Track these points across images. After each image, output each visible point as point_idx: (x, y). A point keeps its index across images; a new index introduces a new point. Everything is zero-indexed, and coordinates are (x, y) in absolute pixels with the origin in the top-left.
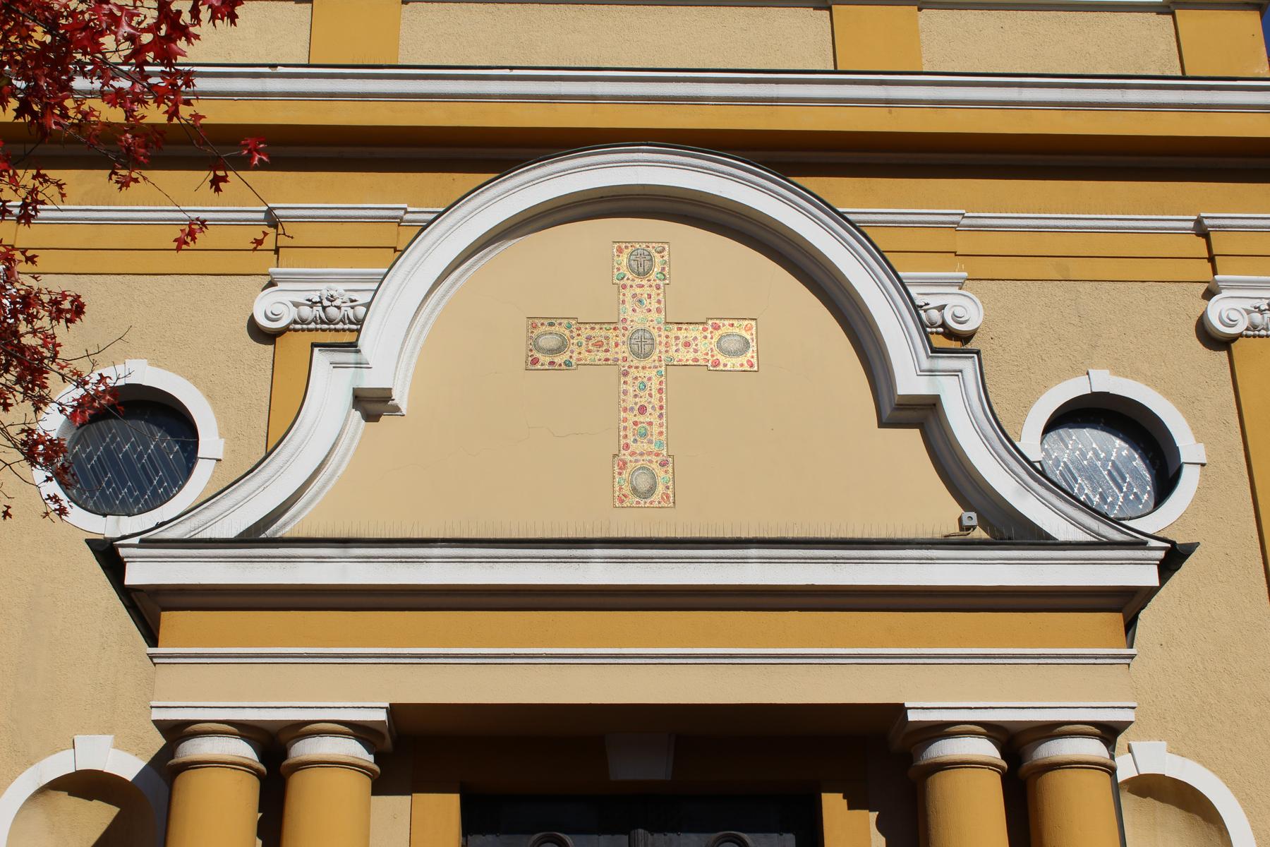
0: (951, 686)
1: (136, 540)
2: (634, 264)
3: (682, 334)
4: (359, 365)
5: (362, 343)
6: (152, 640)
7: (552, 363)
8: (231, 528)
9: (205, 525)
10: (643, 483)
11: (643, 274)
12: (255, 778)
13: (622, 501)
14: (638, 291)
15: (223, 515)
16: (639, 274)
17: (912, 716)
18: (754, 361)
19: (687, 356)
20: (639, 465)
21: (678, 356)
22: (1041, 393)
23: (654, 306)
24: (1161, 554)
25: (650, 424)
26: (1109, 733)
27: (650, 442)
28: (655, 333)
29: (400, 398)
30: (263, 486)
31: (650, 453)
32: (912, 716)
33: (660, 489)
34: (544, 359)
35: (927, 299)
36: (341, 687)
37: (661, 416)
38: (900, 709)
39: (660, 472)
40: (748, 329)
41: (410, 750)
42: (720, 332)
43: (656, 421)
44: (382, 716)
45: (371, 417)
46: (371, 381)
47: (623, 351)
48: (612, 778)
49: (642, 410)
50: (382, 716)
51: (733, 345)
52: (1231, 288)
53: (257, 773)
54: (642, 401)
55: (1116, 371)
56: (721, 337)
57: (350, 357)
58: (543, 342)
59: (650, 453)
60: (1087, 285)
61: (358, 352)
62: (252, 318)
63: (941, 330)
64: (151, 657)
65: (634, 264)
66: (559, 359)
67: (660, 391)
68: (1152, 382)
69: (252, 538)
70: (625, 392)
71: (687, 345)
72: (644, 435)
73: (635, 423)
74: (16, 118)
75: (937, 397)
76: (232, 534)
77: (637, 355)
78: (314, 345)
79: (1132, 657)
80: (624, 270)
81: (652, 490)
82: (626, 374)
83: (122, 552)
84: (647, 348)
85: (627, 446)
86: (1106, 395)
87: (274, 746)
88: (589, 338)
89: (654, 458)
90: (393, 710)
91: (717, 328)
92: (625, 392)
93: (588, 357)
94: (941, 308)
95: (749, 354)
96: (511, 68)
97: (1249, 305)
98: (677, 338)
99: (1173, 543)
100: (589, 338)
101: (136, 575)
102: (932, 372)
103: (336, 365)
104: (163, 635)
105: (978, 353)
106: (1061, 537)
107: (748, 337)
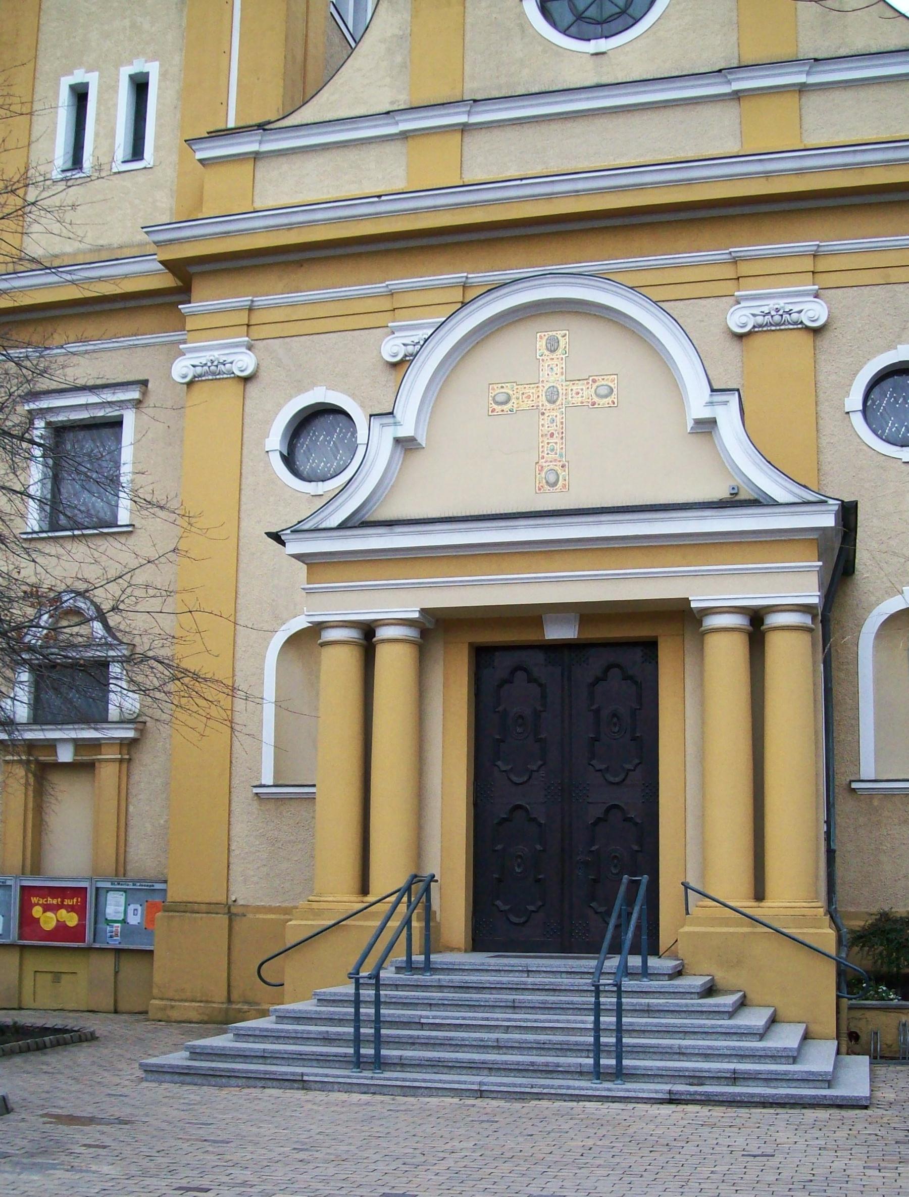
1: (288, 531)
2: (549, 345)
3: (574, 388)
4: (395, 424)
8: (335, 521)
9: (322, 520)
10: (552, 479)
11: (553, 351)
12: (356, 648)
13: (540, 489)
14: (550, 362)
15: (331, 514)
16: (551, 351)
17: (693, 605)
18: (616, 401)
19: (577, 400)
21: (574, 401)
22: (865, 363)
23: (559, 371)
24: (836, 508)
31: (555, 460)
34: (498, 408)
35: (790, 307)
36: (396, 603)
37: (562, 438)
39: (562, 474)
42: (597, 384)
43: (559, 441)
44: (416, 615)
46: (406, 431)
48: (547, 638)
49: (552, 435)
54: (551, 430)
56: (598, 387)
57: (388, 420)
58: (498, 399)
59: (555, 460)
60: (901, 286)
61: (394, 417)
62: (387, 362)
63: (800, 326)
66: (506, 407)
67: (562, 423)
69: (342, 526)
70: (543, 425)
71: (578, 393)
72: (552, 450)
73: (548, 443)
81: (555, 483)
82: (543, 414)
84: (555, 397)
85: (543, 457)
87: (368, 632)
89: (558, 463)
90: (423, 611)
91: (594, 381)
92: (543, 425)
93: (524, 406)
94: (800, 312)
95: (613, 396)
99: (843, 501)
102: (711, 403)
103: (383, 425)
105: (738, 390)
106: (780, 500)
107: (612, 386)
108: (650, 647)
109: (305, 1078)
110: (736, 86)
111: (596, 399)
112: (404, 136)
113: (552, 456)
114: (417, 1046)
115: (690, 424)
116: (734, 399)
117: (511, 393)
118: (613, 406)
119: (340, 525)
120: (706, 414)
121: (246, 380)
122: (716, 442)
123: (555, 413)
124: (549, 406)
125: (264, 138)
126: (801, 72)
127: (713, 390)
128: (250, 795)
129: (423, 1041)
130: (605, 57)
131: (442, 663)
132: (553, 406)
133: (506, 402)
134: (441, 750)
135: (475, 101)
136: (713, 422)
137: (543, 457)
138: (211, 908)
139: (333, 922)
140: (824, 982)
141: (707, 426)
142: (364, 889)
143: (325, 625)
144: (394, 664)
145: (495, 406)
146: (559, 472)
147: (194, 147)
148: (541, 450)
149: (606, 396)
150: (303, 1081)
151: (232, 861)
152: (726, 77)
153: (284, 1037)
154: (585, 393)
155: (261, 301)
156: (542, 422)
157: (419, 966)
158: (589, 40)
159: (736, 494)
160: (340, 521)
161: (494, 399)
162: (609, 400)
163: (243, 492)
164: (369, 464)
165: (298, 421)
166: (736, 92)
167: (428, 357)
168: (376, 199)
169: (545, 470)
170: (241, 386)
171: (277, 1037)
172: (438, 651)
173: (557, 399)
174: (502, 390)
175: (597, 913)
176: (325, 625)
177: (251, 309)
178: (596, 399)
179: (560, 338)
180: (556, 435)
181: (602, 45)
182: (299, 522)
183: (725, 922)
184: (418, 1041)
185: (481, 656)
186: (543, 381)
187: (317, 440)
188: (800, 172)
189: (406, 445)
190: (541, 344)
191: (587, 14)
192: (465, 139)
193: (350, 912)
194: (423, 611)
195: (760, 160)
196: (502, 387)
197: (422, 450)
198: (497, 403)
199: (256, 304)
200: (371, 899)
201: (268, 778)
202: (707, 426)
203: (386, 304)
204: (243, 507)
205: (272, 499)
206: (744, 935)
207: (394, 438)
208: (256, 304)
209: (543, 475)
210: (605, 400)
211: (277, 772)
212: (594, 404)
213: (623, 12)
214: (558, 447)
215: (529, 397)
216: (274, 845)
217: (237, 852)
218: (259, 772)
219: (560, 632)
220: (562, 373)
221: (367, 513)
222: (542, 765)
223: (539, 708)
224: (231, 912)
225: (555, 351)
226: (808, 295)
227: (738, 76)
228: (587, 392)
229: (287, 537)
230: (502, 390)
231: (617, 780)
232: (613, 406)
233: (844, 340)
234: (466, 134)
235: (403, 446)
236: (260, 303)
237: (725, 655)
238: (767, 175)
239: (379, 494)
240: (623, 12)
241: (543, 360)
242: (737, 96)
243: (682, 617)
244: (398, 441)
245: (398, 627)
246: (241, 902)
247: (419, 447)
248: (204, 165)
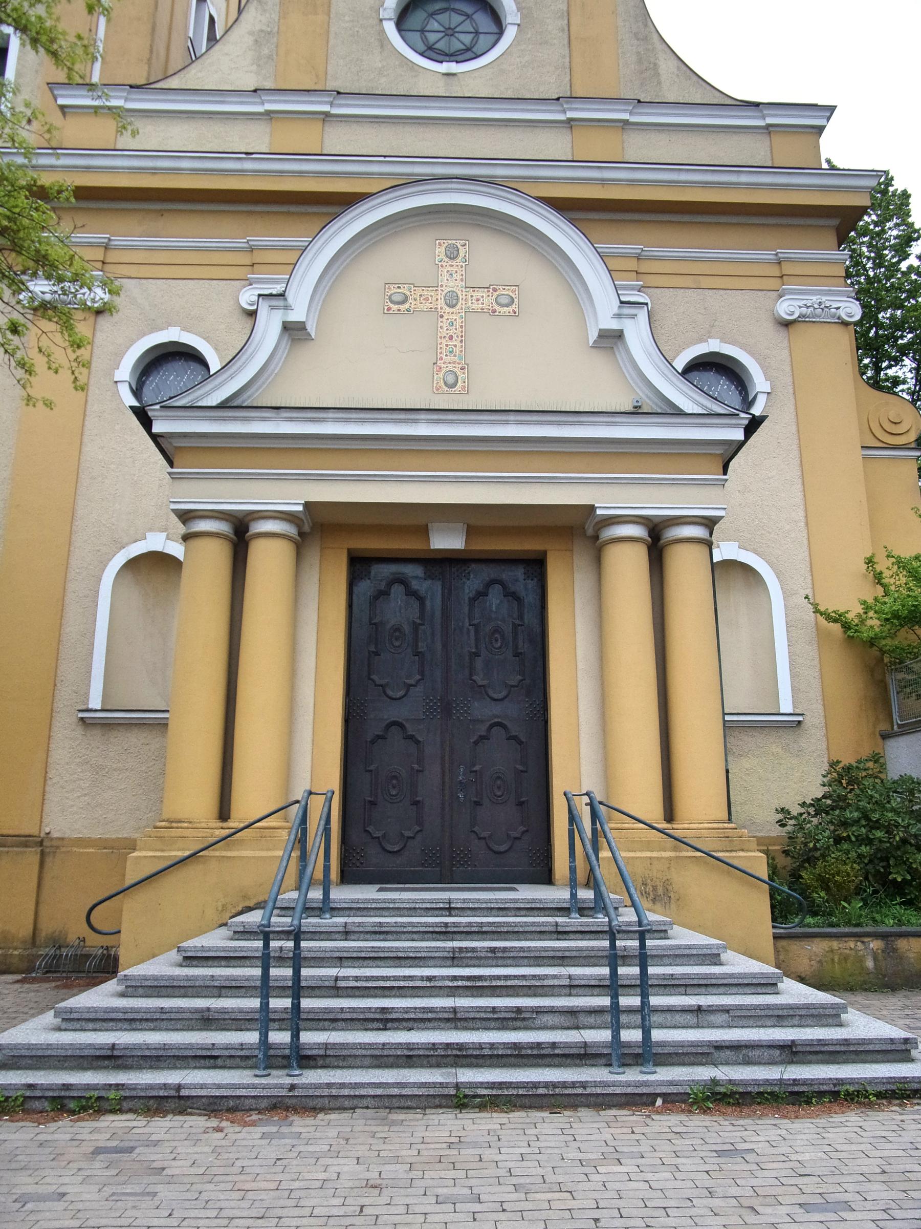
0: (622, 498)
1: (157, 407)
2: (448, 253)
5: (290, 295)
6: (171, 464)
7: (399, 310)
8: (215, 399)
9: (202, 397)
13: (438, 390)
15: (208, 394)
18: (517, 310)
19: (477, 306)
20: (448, 369)
23: (459, 277)
24: (746, 422)
25: (455, 346)
26: (710, 523)
27: (455, 356)
28: (459, 293)
29: (311, 328)
30: (231, 377)
31: (454, 363)
32: (599, 512)
33: (460, 384)
34: (395, 307)
37: (461, 341)
38: (592, 508)
39: (461, 376)
40: (513, 291)
41: (316, 527)
43: (459, 344)
44: (300, 508)
45: (294, 341)
47: (441, 303)
49: (451, 338)
50: (300, 508)
51: (504, 300)
52: (791, 293)
53: (231, 541)
55: (723, 340)
57: (280, 303)
58: (394, 298)
60: (710, 291)
61: (286, 299)
64: (169, 474)
65: (448, 253)
66: (403, 307)
67: (461, 327)
68: (743, 347)
69: (223, 406)
70: (441, 327)
71: (478, 300)
72: (451, 352)
73: (447, 345)
74: (844, 1009)
75: (621, 331)
76: (214, 404)
77: (449, 306)
78: (260, 295)
79: (726, 480)
80: (443, 256)
82: (442, 317)
83: (150, 414)
84: (455, 302)
85: (441, 359)
86: (717, 353)
88: (421, 295)
89: (457, 365)
90: (307, 505)
91: (495, 290)
92: (441, 327)
95: (514, 306)
96: (385, 156)
97: (801, 303)
98: (472, 296)
100: (421, 295)
101: (157, 428)
102: (618, 316)
103: (272, 308)
104: (175, 464)
108: (536, 566)
109: (184, 1093)
110: (570, 115)
111: (496, 307)
112: (269, 115)
113: (450, 358)
114: (340, 1024)
115: (593, 335)
116: (643, 314)
117: (408, 293)
118: (515, 314)
119: (222, 402)
120: (614, 325)
121: (99, 312)
122: (618, 356)
123: (455, 315)
124: (448, 310)
125: (130, 97)
126: (625, 111)
127: (622, 302)
128: (74, 720)
129: (348, 1016)
130: (455, 78)
131: (317, 569)
132: (451, 310)
133: (403, 302)
134: (313, 659)
135: (339, 93)
136: (618, 335)
137: (441, 359)
138: (25, 841)
139: (187, 853)
140: (757, 907)
141: (611, 339)
142: (224, 813)
143: (192, 514)
144: (270, 560)
145: (391, 305)
146: (458, 373)
147: (56, 92)
148: (439, 351)
149: (507, 306)
150: (180, 1098)
151: (47, 789)
152: (562, 106)
153: (141, 1020)
154: (486, 301)
155: (118, 241)
156: (440, 324)
157: (315, 905)
158: (441, 62)
159: (640, 407)
160: (224, 398)
161: (390, 298)
162: (510, 309)
163: (87, 418)
164: (250, 351)
165: (147, 361)
166: (570, 120)
167: (320, 250)
168: (244, 156)
169: (443, 371)
170: (92, 318)
171: (132, 1021)
172: (313, 557)
173: (456, 304)
174: (399, 290)
175: (480, 838)
176: (192, 514)
177: (107, 247)
178: (496, 307)
179: (459, 246)
180: (455, 337)
181: (452, 67)
182: (171, 398)
183: (648, 846)
184: (343, 1016)
185: (359, 565)
186: (442, 286)
187: (166, 380)
188: (632, 183)
189: (294, 332)
190: (440, 251)
191: (436, 46)
192: (326, 128)
193: (212, 840)
194: (307, 505)
195: (599, 167)
196: (399, 287)
197: (312, 343)
198: (392, 302)
199: (112, 243)
200: (233, 824)
201: (95, 702)
202: (611, 339)
203: (246, 259)
204: (87, 432)
205: (117, 427)
206: (670, 859)
207: (284, 323)
208: (112, 243)
209: (441, 375)
210: (505, 309)
211: (106, 695)
212: (494, 311)
213: (468, 49)
214: (457, 350)
215: (427, 299)
216: (97, 773)
217: (55, 780)
218: (87, 694)
219: (448, 540)
220: (462, 280)
221: (249, 397)
222: (420, 680)
223: (418, 621)
224: (43, 847)
225: (454, 258)
226: (633, 289)
227: (574, 106)
228: (488, 300)
229: (156, 413)
230: (399, 290)
231: (501, 696)
232: (515, 314)
233: (663, 331)
234: (327, 124)
235: (290, 335)
236: (116, 243)
237: (627, 566)
238: (603, 182)
239: (272, 367)
240: (468, 49)
241: (442, 266)
242: (570, 123)
243: (581, 530)
244: (287, 327)
245: (277, 522)
246: (55, 835)
247: (308, 338)
248: (64, 114)
